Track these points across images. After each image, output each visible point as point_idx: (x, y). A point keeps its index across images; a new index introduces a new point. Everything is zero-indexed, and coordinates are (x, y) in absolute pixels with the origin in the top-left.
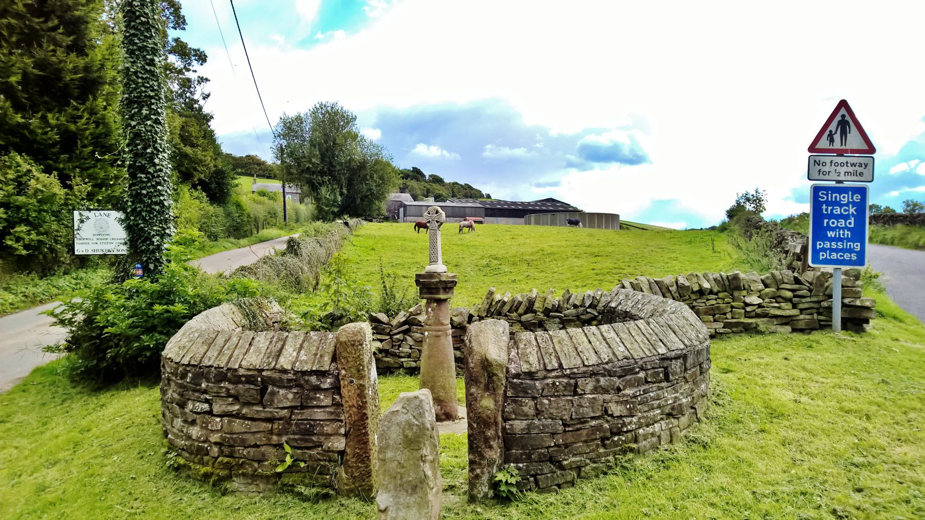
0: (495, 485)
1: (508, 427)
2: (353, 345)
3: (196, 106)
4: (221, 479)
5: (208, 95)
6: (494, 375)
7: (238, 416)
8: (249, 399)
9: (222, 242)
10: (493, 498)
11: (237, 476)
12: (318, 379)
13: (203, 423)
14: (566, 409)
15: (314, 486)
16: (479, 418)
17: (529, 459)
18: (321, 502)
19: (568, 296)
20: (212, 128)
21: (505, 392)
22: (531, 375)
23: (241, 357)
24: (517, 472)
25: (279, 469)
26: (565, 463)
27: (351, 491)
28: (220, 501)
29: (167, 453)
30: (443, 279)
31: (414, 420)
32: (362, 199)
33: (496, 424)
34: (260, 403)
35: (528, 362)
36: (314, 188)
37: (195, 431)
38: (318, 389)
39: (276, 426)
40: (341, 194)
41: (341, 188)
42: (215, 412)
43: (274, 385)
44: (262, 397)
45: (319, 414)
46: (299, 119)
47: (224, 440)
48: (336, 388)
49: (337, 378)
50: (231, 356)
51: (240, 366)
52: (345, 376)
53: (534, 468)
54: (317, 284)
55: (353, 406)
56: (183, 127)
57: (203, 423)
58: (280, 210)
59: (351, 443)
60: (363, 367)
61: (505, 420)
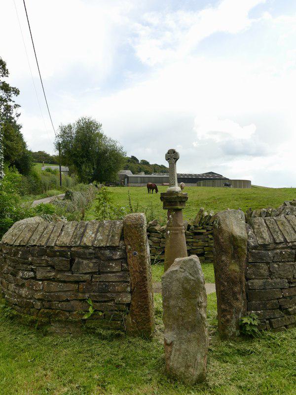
0: (241, 327)
1: (249, 284)
2: (136, 227)
3: (13, 121)
4: (43, 324)
5: (19, 115)
6: (238, 247)
7: (54, 280)
8: (62, 267)
9: (26, 197)
10: (239, 336)
11: (55, 322)
12: (111, 253)
13: (30, 285)
14: (290, 271)
15: (109, 329)
16: (228, 278)
17: (265, 308)
18: (114, 340)
19: (250, 212)
20: (21, 133)
21: (247, 259)
22: (264, 246)
23: (56, 238)
24: (257, 317)
25: (86, 317)
26: (290, 310)
27: (136, 332)
28: (43, 339)
29: (5, 307)
30: (180, 195)
31: (190, 277)
32: (105, 171)
33: (241, 282)
34: (70, 270)
35: (262, 238)
36: (78, 165)
37: (24, 292)
38: (111, 260)
39: (81, 286)
40: (94, 169)
41: (93, 165)
42: (38, 278)
43: (79, 257)
44: (71, 266)
45: (112, 277)
46: (70, 127)
47: (45, 297)
48: (124, 259)
49: (125, 251)
50: (49, 238)
51: (56, 245)
52: (130, 250)
53: (268, 314)
54: (83, 217)
55: (136, 271)
56: (6, 130)
57: (30, 285)
58: (58, 179)
59: (135, 298)
60: (143, 242)
61: (247, 279)
